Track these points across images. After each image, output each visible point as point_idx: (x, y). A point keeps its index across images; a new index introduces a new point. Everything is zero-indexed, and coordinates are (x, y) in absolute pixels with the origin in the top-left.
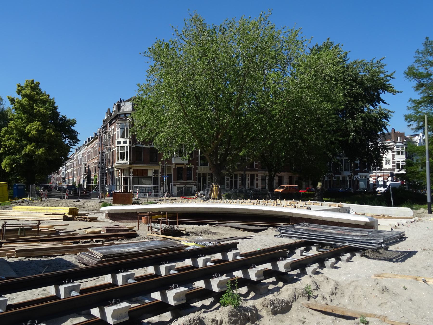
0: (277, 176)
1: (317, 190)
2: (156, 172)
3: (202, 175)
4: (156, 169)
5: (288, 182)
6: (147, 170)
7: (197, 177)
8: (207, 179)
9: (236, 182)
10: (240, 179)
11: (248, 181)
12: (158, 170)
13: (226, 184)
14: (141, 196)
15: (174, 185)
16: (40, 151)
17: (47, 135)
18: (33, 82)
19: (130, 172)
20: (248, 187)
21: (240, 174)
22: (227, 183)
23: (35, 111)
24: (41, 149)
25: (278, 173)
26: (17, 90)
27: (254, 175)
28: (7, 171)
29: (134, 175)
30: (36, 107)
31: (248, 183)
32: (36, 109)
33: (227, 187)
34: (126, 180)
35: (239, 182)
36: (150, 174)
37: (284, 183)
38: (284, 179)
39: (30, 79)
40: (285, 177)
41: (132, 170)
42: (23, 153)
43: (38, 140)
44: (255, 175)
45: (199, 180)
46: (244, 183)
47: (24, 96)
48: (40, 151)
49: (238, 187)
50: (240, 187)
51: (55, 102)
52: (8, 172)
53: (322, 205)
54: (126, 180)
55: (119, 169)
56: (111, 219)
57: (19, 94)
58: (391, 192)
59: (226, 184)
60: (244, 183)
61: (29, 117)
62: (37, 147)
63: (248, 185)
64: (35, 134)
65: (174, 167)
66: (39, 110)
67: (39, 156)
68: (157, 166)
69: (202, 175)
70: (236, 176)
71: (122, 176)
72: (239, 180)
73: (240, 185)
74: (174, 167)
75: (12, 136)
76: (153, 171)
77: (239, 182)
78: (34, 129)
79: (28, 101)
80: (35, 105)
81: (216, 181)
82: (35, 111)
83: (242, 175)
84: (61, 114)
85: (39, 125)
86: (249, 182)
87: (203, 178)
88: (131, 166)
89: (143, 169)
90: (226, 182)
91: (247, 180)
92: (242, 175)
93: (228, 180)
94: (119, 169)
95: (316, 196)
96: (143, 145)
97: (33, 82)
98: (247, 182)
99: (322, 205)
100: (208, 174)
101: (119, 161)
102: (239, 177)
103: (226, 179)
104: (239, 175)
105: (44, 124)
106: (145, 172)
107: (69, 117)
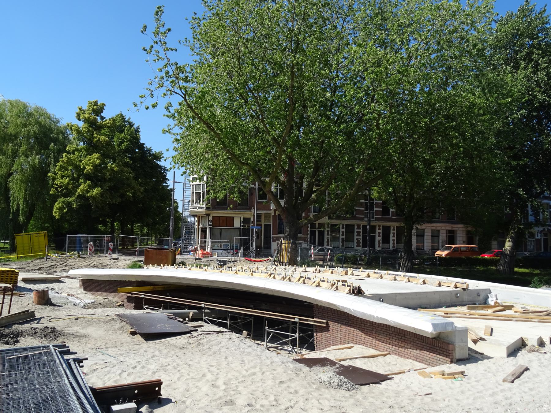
1: (503, 254)
2: (246, 221)
3: (317, 226)
4: (247, 216)
5: (465, 240)
6: (233, 217)
7: (309, 229)
8: (326, 233)
9: (373, 239)
11: (394, 236)
12: (250, 218)
13: (355, 241)
14: (224, 255)
15: (274, 241)
16: (96, 191)
17: (109, 171)
18: (96, 103)
19: (209, 221)
20: (394, 247)
21: (379, 226)
22: (357, 239)
23: (95, 140)
24: (96, 189)
25: (418, 223)
26: (76, 115)
27: (389, 227)
28: (57, 217)
29: (213, 225)
30: (95, 135)
31: (394, 240)
32: (96, 138)
33: (358, 245)
34: (204, 231)
35: (378, 239)
36: (237, 223)
37: (458, 242)
38: (458, 235)
39: (93, 100)
40: (458, 232)
41: (211, 218)
42: (77, 194)
43: (95, 177)
44: (356, 227)
45: (313, 233)
46: (386, 239)
47: (85, 121)
48: (96, 191)
49: (377, 245)
50: (379, 246)
51: (137, 131)
52: (58, 219)
53: (424, 283)
54: (204, 231)
55: (196, 216)
56: (85, 289)
57: (79, 120)
59: (355, 241)
60: (386, 239)
61: (89, 148)
62: (91, 187)
63: (394, 243)
64: (91, 169)
65: (273, 214)
67: (94, 198)
68: (248, 212)
69: (317, 226)
70: (373, 228)
71: (199, 226)
72: (377, 235)
73: (379, 243)
74: (273, 214)
75: (66, 172)
76: (242, 220)
77: (378, 239)
78: (90, 163)
79: (86, 127)
80: (95, 132)
81: (288, 235)
82: (95, 140)
83: (364, 227)
84: (145, 146)
85: (97, 158)
86: (395, 238)
87: (318, 231)
88: (209, 212)
89: (227, 217)
90: (356, 237)
91: (391, 235)
92: (364, 227)
93: (358, 234)
94: (196, 216)
95: (501, 265)
97: (96, 103)
98: (392, 239)
99: (424, 283)
100: (326, 226)
101: (194, 206)
103: (356, 234)
104: (377, 228)
105: (104, 156)
106: (229, 221)
107: (155, 150)
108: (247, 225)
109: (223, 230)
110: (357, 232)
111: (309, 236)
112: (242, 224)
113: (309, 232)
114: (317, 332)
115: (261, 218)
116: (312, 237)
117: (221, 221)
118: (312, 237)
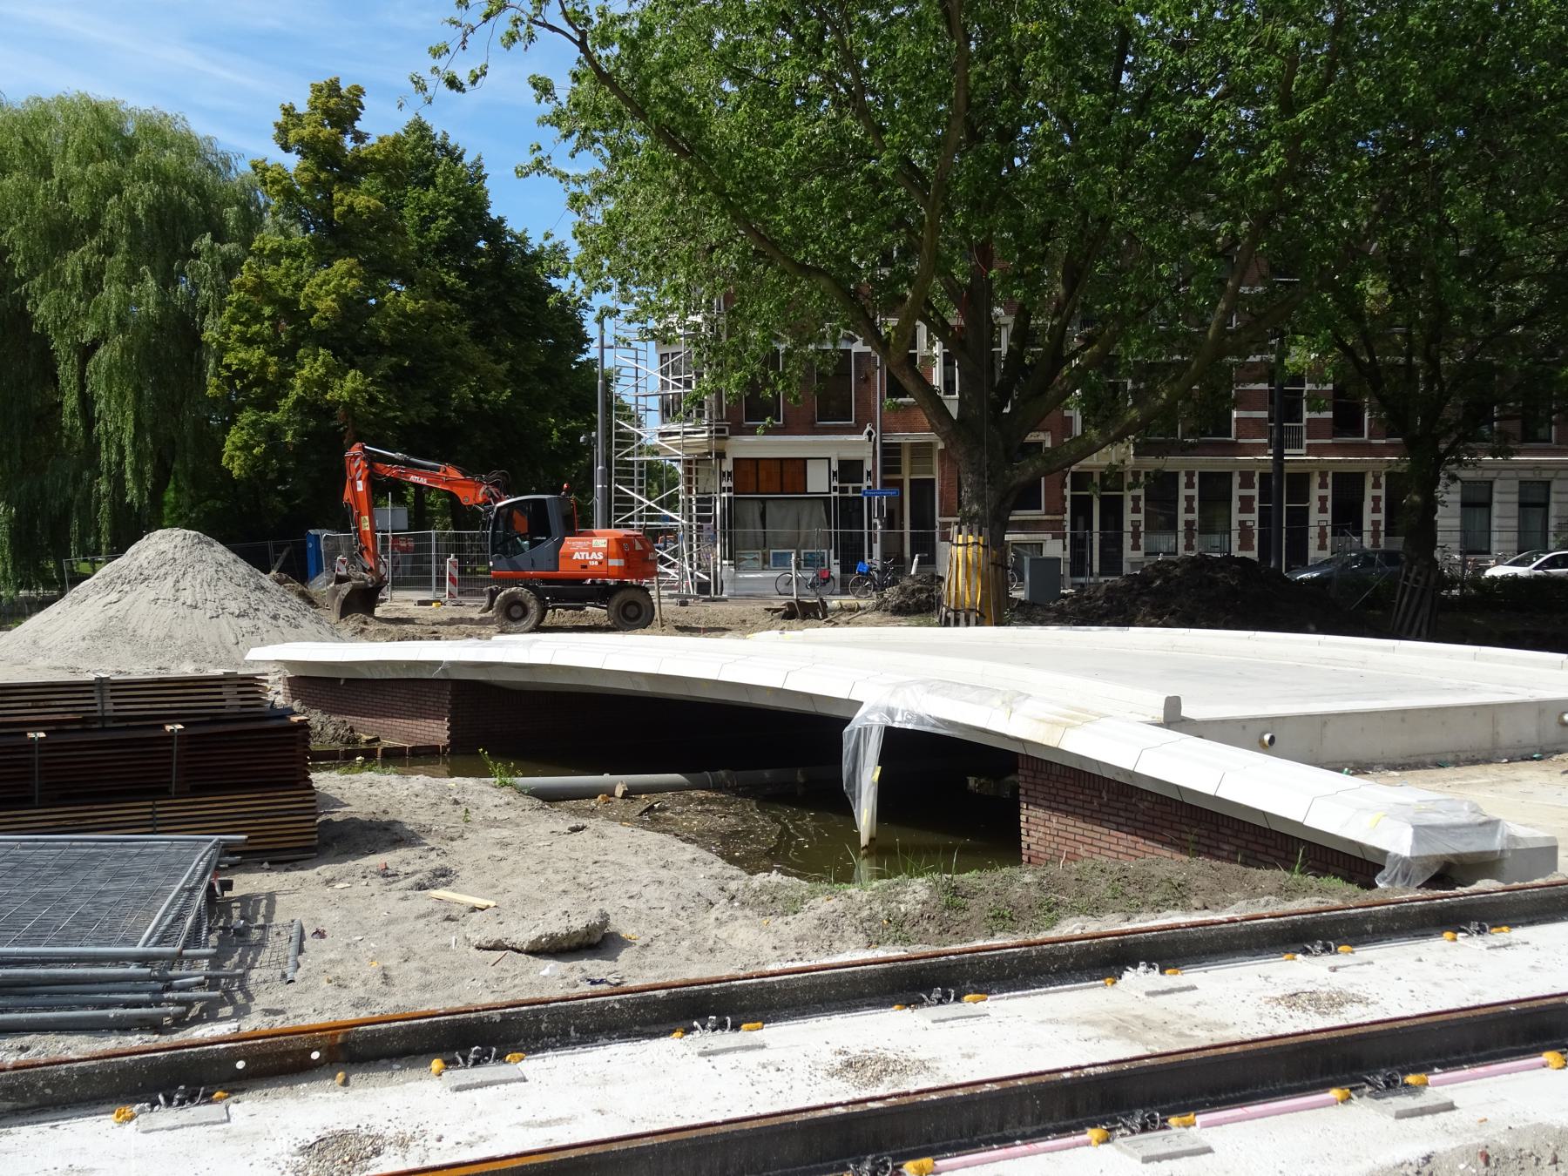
0: (1453, 478)
6: (805, 460)
7: (1067, 492)
8: (1128, 505)
10: (1323, 499)
19: (722, 474)
22: (1242, 523)
35: (1319, 518)
36: (818, 481)
41: (728, 466)
44: (1236, 480)
45: (1081, 508)
51: (485, 176)
58: (767, 774)
66: (351, 206)
72: (1314, 505)
73: (1322, 535)
76: (835, 467)
87: (1103, 499)
90: (1236, 517)
93: (1246, 504)
96: (852, 340)
102: (1315, 492)
103: (1236, 504)
108: (850, 486)
109: (770, 506)
110: (1241, 498)
111: (1068, 516)
112: (835, 483)
113: (1068, 504)
114: (317, 769)
115: (899, 461)
116: (1081, 520)
117: (762, 475)
118: (1081, 520)
